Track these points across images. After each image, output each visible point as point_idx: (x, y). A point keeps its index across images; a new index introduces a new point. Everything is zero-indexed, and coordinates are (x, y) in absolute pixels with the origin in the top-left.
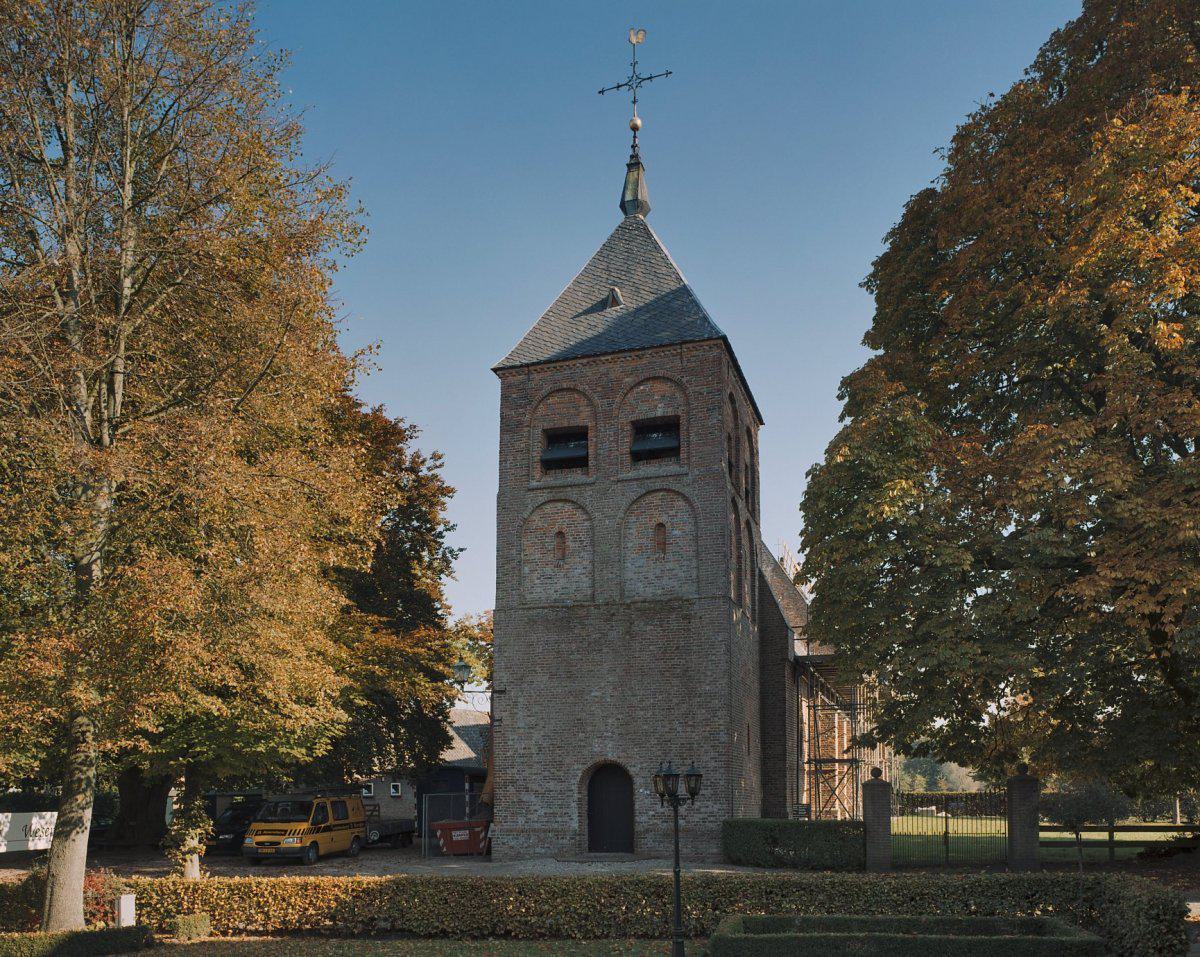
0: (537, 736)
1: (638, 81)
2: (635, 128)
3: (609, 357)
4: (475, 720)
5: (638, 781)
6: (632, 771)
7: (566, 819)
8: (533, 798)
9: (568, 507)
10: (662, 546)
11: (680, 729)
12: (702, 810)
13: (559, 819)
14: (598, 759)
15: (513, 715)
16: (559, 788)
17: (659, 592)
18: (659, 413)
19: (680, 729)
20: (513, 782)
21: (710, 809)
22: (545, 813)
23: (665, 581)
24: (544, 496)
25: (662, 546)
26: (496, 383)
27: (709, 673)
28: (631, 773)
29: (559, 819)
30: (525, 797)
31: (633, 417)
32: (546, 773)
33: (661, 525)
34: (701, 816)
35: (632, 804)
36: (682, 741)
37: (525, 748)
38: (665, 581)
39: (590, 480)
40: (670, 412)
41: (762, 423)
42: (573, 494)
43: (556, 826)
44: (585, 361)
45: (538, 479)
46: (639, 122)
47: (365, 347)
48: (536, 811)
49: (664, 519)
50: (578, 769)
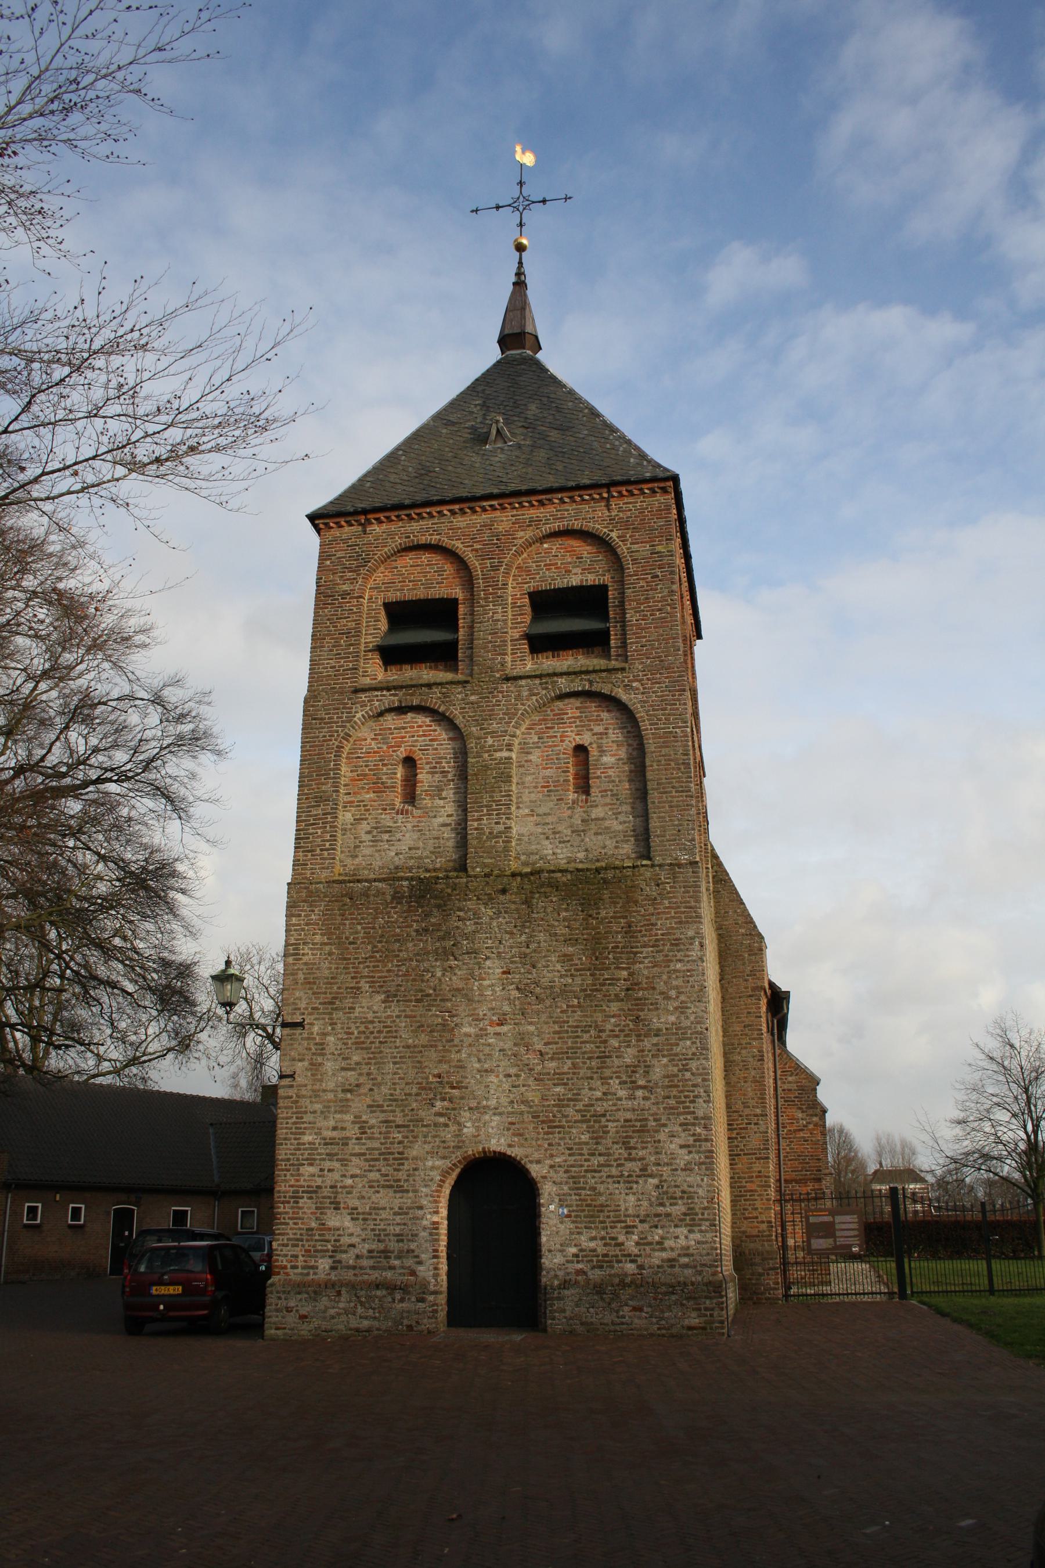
0: (359, 1104)
1: (527, 203)
2: (520, 248)
3: (495, 503)
4: (428, 586)
5: (547, 1190)
6: (536, 1171)
7: (409, 1262)
8: (347, 1223)
9: (422, 719)
10: (584, 785)
11: (622, 1093)
12: (668, 1243)
13: (397, 1263)
14: (472, 1150)
15: (315, 1067)
16: (397, 1203)
17: (581, 855)
18: (575, 581)
19: (622, 1093)
20: (313, 1192)
21: (682, 1242)
22: (370, 1251)
23: (590, 840)
24: (390, 699)
25: (584, 785)
26: (311, 541)
27: (673, 993)
28: (534, 1174)
29: (397, 1263)
30: (333, 1220)
31: (532, 586)
32: (374, 1175)
33: (581, 750)
34: (664, 1255)
35: (534, 1233)
36: (629, 1115)
37: (335, 1129)
38: (590, 840)
39: (460, 677)
40: (591, 579)
41: (699, 636)
42: (434, 698)
43: (389, 1274)
44: (456, 507)
45: (375, 671)
46: (525, 241)
47: (14, 22)
48: (353, 1246)
49: (586, 739)
50: (432, 1168)
